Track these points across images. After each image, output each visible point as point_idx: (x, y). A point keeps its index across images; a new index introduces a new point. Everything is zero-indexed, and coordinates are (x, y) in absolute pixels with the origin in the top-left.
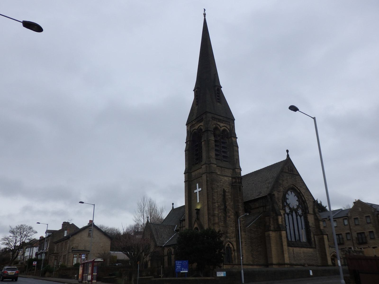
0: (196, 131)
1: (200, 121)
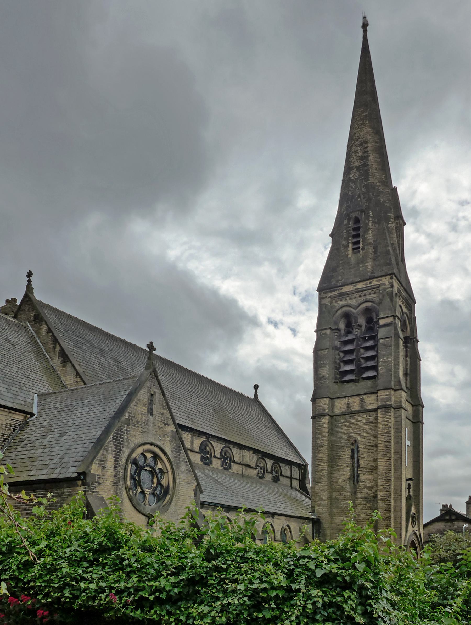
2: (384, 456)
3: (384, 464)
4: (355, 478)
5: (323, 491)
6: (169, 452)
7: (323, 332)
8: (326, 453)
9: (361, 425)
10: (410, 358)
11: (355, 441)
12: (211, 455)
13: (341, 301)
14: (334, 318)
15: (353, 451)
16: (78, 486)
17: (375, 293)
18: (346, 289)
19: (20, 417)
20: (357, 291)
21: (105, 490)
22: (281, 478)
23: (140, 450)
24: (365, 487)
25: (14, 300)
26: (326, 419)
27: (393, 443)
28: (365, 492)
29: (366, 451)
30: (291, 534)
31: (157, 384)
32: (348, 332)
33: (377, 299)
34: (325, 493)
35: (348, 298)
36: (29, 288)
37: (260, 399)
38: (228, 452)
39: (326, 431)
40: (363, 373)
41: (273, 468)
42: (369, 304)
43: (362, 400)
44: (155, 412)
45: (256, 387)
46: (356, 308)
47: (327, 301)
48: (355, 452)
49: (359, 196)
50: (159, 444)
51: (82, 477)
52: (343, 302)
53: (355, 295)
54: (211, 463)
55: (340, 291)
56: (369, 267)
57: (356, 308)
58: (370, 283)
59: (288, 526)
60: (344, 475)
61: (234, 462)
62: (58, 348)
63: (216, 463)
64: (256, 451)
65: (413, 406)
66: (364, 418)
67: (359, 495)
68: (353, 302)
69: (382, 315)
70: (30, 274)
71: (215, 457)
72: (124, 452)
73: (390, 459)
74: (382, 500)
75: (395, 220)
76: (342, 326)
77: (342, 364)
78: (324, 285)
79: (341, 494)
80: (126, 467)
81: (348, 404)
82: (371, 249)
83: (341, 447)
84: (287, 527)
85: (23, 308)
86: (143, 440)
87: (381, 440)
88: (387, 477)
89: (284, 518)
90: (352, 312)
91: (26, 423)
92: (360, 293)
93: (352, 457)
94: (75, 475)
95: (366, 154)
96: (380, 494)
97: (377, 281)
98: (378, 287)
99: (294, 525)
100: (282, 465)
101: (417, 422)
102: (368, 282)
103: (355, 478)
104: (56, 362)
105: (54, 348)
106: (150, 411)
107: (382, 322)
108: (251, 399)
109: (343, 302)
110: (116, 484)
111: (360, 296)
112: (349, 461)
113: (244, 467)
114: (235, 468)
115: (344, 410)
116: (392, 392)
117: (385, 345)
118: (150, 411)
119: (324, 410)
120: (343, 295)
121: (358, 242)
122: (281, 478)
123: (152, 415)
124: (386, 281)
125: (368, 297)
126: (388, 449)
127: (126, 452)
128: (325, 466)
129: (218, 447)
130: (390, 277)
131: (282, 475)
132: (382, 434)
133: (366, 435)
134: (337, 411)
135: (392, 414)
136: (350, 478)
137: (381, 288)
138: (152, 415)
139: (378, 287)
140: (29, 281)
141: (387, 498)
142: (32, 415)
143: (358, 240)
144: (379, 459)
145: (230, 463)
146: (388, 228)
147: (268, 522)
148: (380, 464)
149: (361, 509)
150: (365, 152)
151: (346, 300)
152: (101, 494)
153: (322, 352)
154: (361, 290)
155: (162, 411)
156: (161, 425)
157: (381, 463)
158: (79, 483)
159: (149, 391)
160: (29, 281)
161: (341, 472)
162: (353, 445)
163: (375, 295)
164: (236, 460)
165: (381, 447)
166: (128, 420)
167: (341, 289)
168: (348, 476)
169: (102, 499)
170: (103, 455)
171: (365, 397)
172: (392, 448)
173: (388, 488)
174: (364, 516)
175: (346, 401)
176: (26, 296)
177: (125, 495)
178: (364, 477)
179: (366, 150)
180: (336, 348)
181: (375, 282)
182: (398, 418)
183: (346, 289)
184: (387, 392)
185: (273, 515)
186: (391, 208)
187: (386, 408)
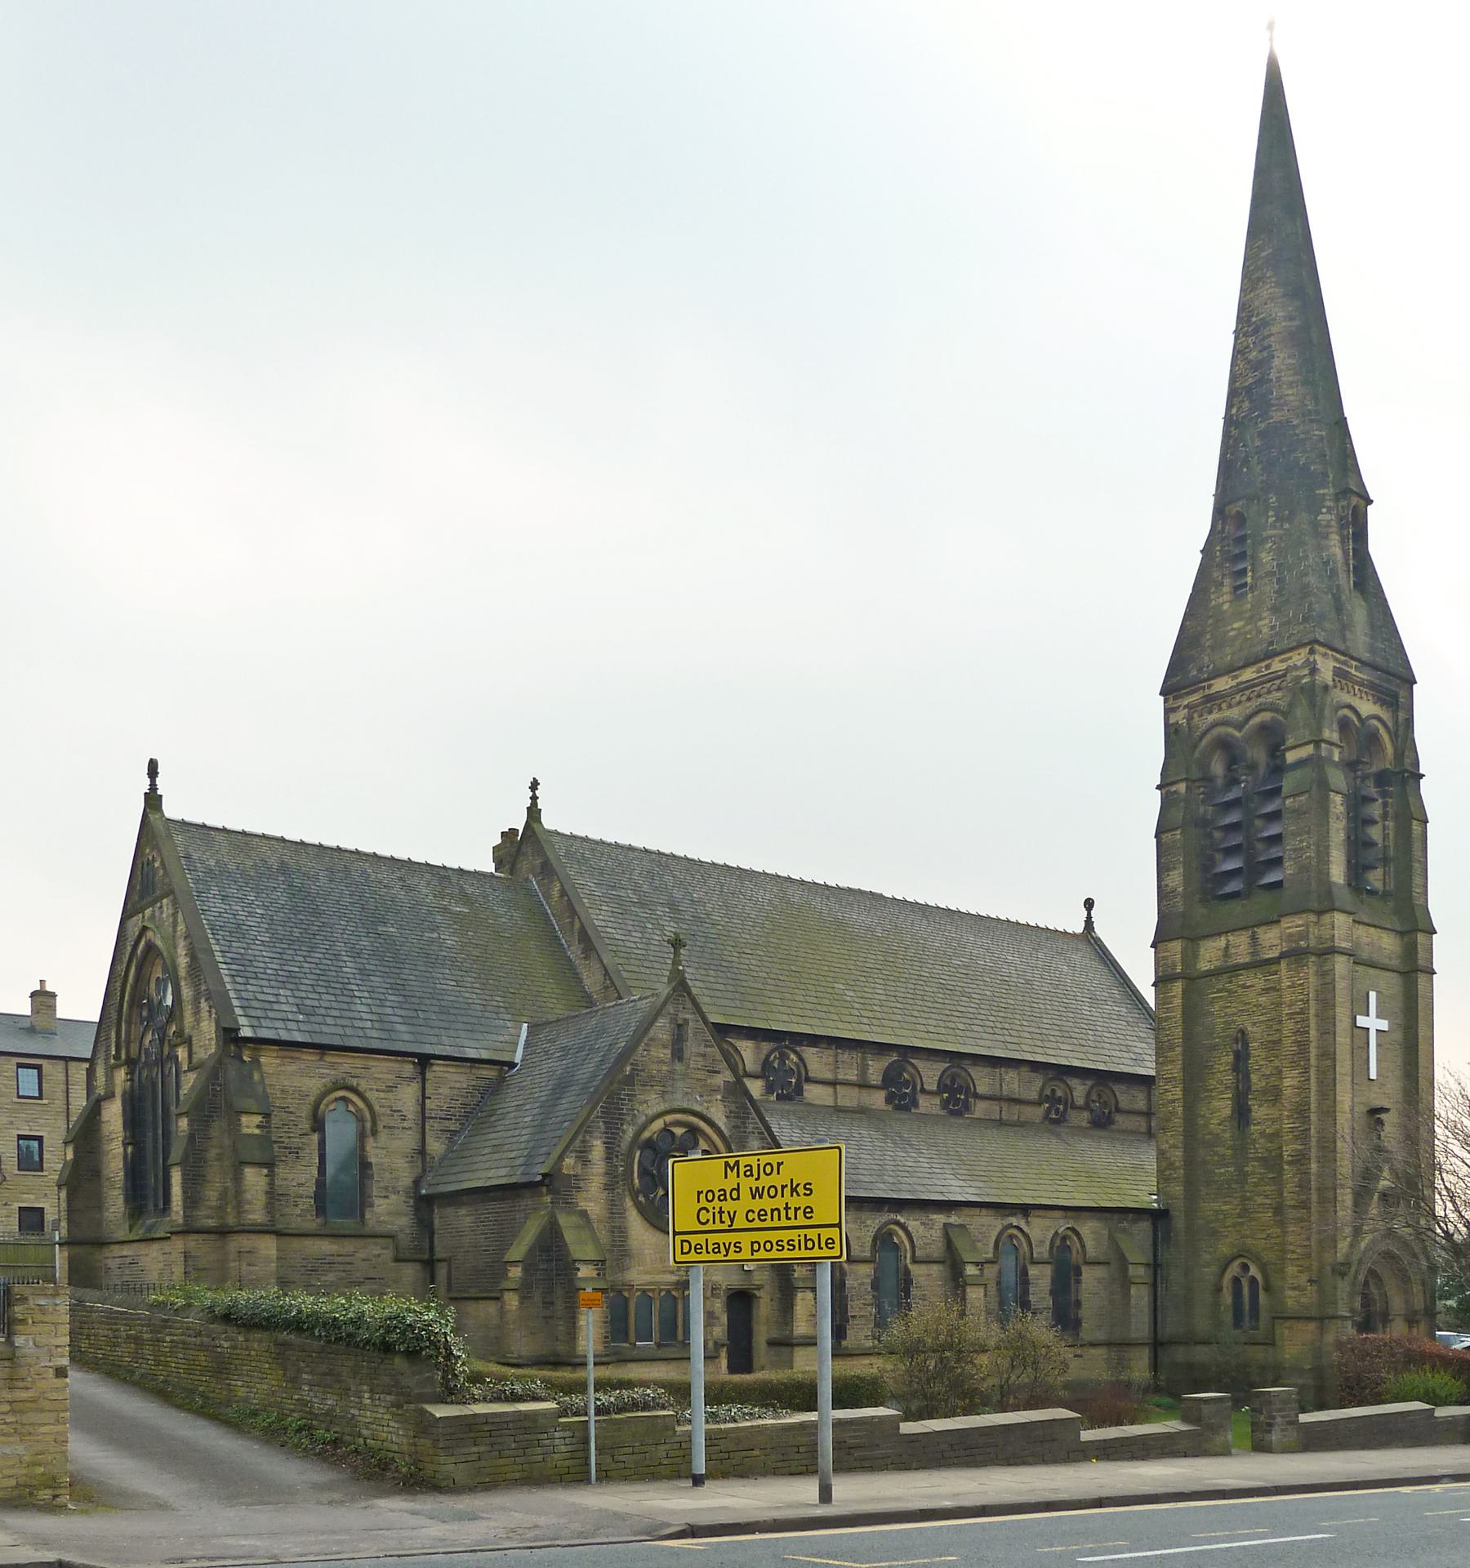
2: (1294, 1065)
3: (1295, 1083)
4: (1242, 1114)
5: (1174, 1146)
6: (721, 1122)
7: (1173, 789)
8: (1179, 1064)
9: (1252, 997)
10: (1396, 817)
11: (1242, 1032)
12: (914, 1087)
13: (1210, 712)
14: (1197, 755)
15: (1237, 1055)
16: (542, 1195)
17: (1279, 689)
18: (1222, 684)
19: (490, 1073)
20: (1241, 688)
21: (593, 1200)
22: (1118, 1118)
23: (658, 1125)
24: (1262, 1134)
25: (513, 831)
26: (1178, 987)
27: (1313, 1033)
28: (1261, 1147)
29: (1263, 1055)
30: (1083, 1246)
31: (689, 1005)
32: (1233, 781)
33: (1283, 704)
34: (1179, 1153)
35: (1224, 705)
36: (534, 812)
37: (1100, 930)
38: (959, 1076)
39: (1178, 1014)
40: (1262, 874)
41: (1094, 1097)
42: (1266, 716)
43: (1254, 938)
44: (687, 1054)
45: (1089, 904)
46: (1239, 727)
47: (1179, 717)
48: (1241, 1060)
49: (1246, 462)
50: (697, 1108)
51: (550, 1181)
52: (1215, 716)
53: (1238, 697)
54: (915, 1104)
55: (1207, 692)
56: (1265, 630)
57: (1239, 727)
58: (1268, 667)
59: (1073, 1229)
60: (1219, 1110)
61: (977, 1096)
62: (577, 925)
63: (928, 1105)
64: (1035, 1066)
65: (1401, 934)
66: (1257, 980)
67: (1251, 1153)
68: (1235, 713)
69: (1290, 742)
70: (534, 785)
71: (923, 1091)
72: (624, 1132)
73: (1306, 1071)
74: (1290, 1163)
75: (1337, 500)
76: (1218, 768)
77: (1219, 856)
78: (1174, 680)
79: (1216, 1153)
80: (630, 1155)
81: (1227, 947)
82: (1269, 588)
83: (1214, 1047)
84: (1069, 1233)
85: (524, 849)
86: (662, 1107)
87: (1289, 1027)
88: (1301, 1112)
89: (1057, 1214)
90: (1232, 736)
91: (501, 1080)
92: (1247, 692)
93: (1236, 1068)
94: (539, 1178)
95: (1265, 354)
96: (1288, 1151)
97: (1282, 661)
98: (1284, 675)
99: (1089, 1229)
100: (1119, 1089)
101: (1412, 974)
102: (1263, 664)
103: (1242, 1114)
104: (574, 952)
105: (572, 924)
106: (678, 1054)
107: (1291, 757)
108: (1074, 935)
109: (1215, 716)
110: (609, 1187)
111: (1249, 699)
112: (1229, 1078)
113: (1005, 1106)
114: (980, 1109)
115: (1218, 964)
116: (1312, 918)
117: (1295, 811)
118: (678, 1054)
119: (1174, 967)
120: (1213, 701)
121: (1243, 572)
122: (1118, 1118)
123: (680, 1059)
124: (1298, 658)
125: (1270, 698)
126: (1303, 1047)
127: (630, 1131)
128: (1178, 1092)
129: (930, 1074)
130: (1307, 649)
131: (1118, 1110)
132: (1291, 1016)
133: (1262, 1018)
134: (1204, 966)
135: (1312, 970)
136: (1231, 1117)
137: (1289, 678)
138: (680, 1059)
139: (1284, 675)
140: (534, 798)
141: (1300, 1159)
142: (512, 1065)
143: (1240, 566)
144: (1286, 1073)
145: (966, 1100)
146: (1315, 525)
147: (1011, 1226)
148: (1287, 1082)
149: (1256, 1185)
150: (1265, 349)
151: (1220, 709)
152: (583, 1205)
153: (1169, 835)
154: (1250, 685)
155: (702, 1049)
156: (702, 1075)
157: (1290, 1081)
158: (544, 1189)
159: (673, 1020)
160: (534, 798)
161: (1216, 1104)
162: (1236, 1041)
163: (1280, 694)
164: (981, 1090)
165: (1289, 1046)
166: (632, 1076)
167: (1210, 687)
168: (1228, 1112)
169: (584, 1214)
170: (583, 1141)
171: (1260, 931)
172: (1313, 1045)
173: (1303, 1136)
174: (1260, 1200)
175: (1222, 942)
176: (527, 826)
177: (629, 1203)
178: (1259, 1112)
179: (1266, 343)
180: (1204, 823)
181: (1277, 665)
182: (1326, 975)
183: (1222, 684)
184: (1299, 920)
185: (1025, 1210)
186: (1326, 475)
187: (1295, 955)
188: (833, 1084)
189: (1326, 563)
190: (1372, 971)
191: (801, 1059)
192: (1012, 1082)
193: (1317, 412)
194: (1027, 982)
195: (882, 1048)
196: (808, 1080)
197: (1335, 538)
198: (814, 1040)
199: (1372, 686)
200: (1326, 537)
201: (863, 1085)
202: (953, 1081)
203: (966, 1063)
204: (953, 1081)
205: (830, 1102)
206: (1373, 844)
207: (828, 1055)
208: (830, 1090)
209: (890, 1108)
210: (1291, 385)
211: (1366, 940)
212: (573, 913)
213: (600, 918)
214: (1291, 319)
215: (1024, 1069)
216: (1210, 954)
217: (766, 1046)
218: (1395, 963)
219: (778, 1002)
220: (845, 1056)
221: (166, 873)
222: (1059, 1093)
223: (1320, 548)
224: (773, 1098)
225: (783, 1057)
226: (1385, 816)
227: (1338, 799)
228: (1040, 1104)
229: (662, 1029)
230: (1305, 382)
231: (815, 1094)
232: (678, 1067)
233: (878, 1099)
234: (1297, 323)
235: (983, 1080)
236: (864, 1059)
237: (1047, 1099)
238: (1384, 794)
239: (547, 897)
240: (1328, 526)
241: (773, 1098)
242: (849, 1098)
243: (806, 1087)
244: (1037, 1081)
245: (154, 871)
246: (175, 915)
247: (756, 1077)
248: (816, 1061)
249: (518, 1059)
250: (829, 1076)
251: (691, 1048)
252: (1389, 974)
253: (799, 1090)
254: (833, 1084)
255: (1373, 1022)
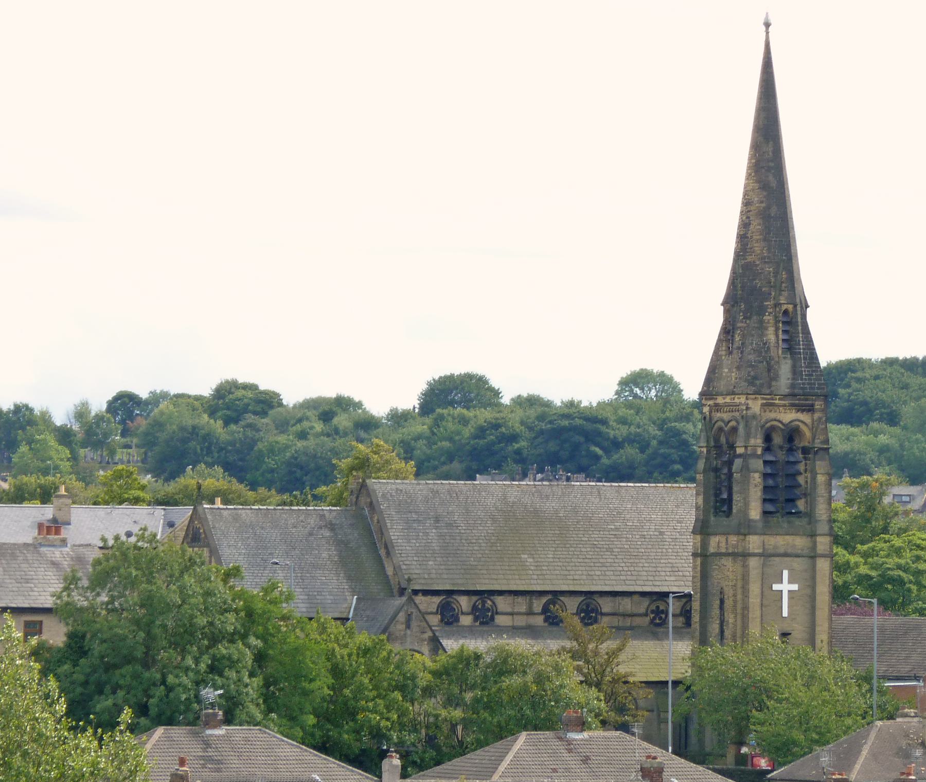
0: (780, 425)
1: (801, 408)
61: (602, 614)
64: (643, 594)
104: (382, 552)
106: (408, 626)
113: (621, 618)
118: (408, 626)
129: (572, 604)
134: (712, 549)
188: (512, 614)
189: (765, 344)
190: (786, 559)
191: (494, 603)
192: (626, 605)
193: (769, 258)
194: (661, 533)
195: (542, 593)
196: (497, 613)
197: (771, 330)
198: (501, 593)
199: (793, 405)
200: (766, 329)
201: (530, 613)
202: (588, 606)
203: (596, 597)
204: (588, 606)
205: (510, 624)
206: (800, 486)
207: (509, 599)
208: (510, 617)
209: (546, 624)
210: (757, 241)
211: (782, 543)
212: (382, 534)
213: (395, 533)
214: (762, 202)
215: (636, 597)
216: (716, 543)
217: (474, 598)
218: (806, 552)
219: (485, 572)
220: (520, 599)
221: (206, 536)
222: (661, 608)
223: (762, 335)
224: (477, 624)
225: (484, 603)
226: (806, 471)
227: (757, 475)
228: (646, 615)
229: (401, 617)
230: (765, 240)
231: (500, 620)
232: (408, 632)
233: (539, 620)
234: (763, 205)
235: (606, 605)
236: (530, 600)
237: (652, 612)
238: (805, 459)
239: (372, 521)
240: (768, 323)
241: (477, 624)
242: (521, 621)
243: (496, 617)
244: (646, 602)
245: (200, 534)
246: (210, 557)
247: (468, 614)
248: (502, 603)
249: (351, 616)
250: (509, 610)
251: (414, 624)
252: (799, 560)
253: (492, 619)
254: (512, 614)
255: (786, 587)
